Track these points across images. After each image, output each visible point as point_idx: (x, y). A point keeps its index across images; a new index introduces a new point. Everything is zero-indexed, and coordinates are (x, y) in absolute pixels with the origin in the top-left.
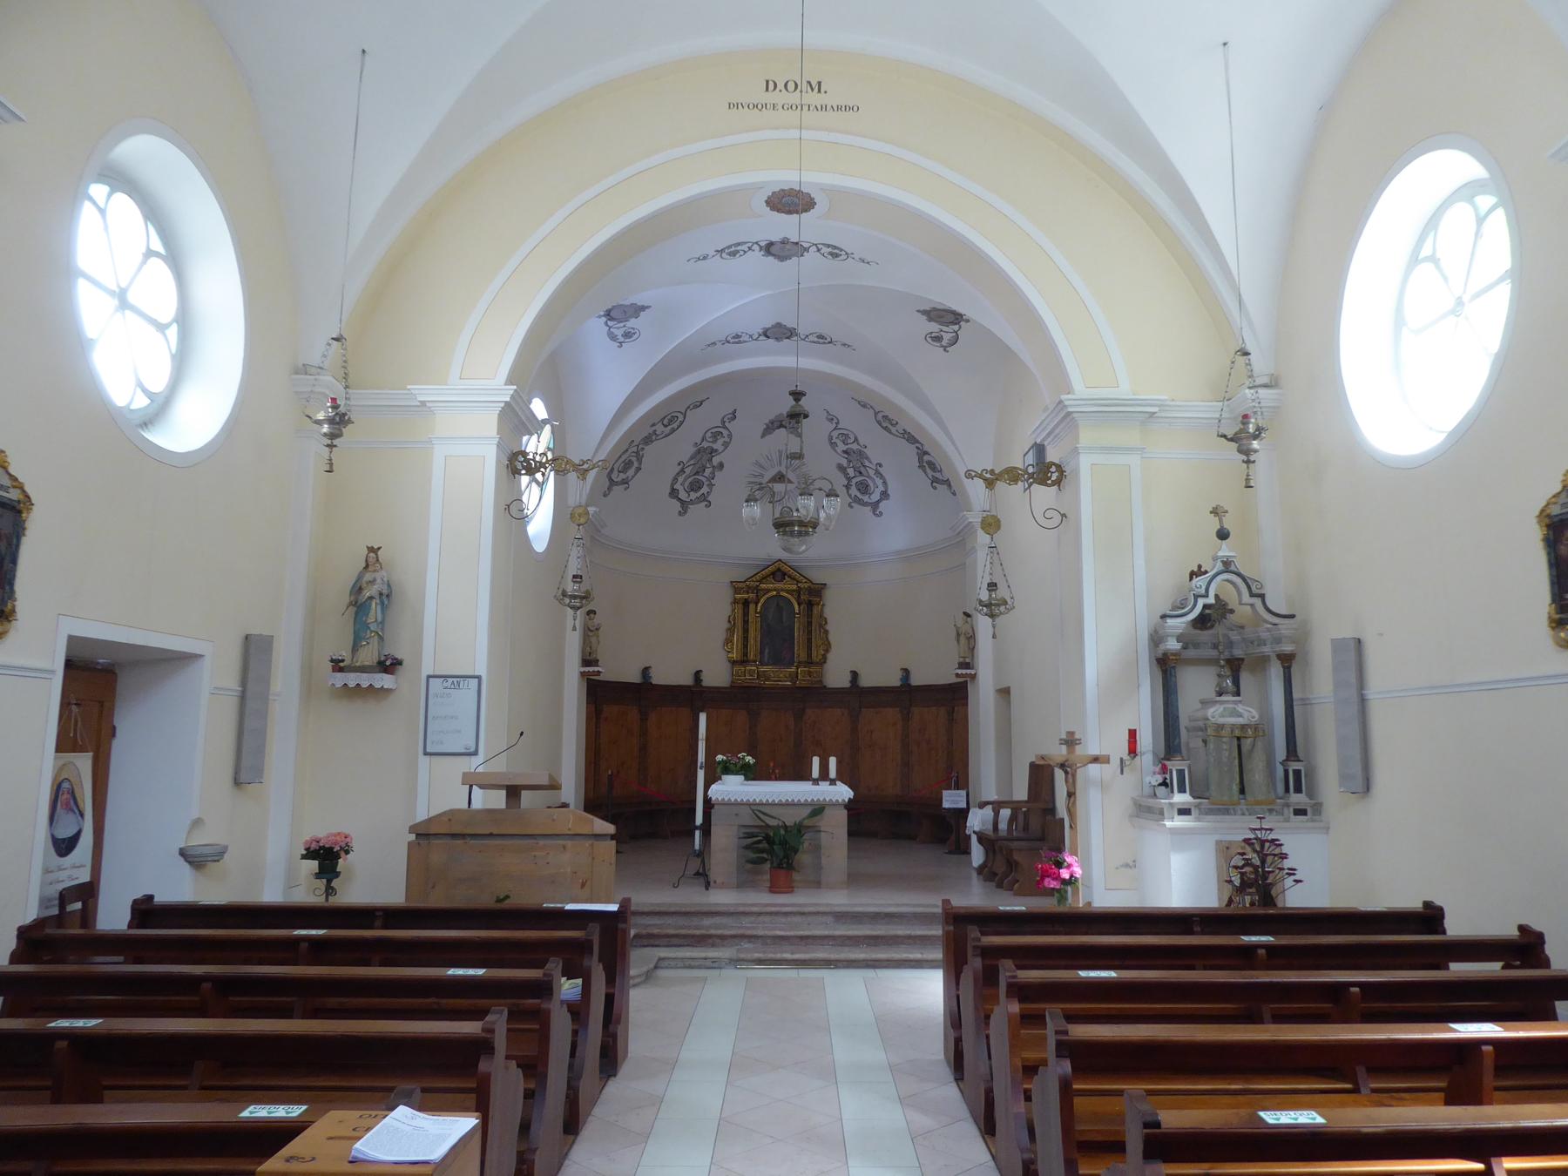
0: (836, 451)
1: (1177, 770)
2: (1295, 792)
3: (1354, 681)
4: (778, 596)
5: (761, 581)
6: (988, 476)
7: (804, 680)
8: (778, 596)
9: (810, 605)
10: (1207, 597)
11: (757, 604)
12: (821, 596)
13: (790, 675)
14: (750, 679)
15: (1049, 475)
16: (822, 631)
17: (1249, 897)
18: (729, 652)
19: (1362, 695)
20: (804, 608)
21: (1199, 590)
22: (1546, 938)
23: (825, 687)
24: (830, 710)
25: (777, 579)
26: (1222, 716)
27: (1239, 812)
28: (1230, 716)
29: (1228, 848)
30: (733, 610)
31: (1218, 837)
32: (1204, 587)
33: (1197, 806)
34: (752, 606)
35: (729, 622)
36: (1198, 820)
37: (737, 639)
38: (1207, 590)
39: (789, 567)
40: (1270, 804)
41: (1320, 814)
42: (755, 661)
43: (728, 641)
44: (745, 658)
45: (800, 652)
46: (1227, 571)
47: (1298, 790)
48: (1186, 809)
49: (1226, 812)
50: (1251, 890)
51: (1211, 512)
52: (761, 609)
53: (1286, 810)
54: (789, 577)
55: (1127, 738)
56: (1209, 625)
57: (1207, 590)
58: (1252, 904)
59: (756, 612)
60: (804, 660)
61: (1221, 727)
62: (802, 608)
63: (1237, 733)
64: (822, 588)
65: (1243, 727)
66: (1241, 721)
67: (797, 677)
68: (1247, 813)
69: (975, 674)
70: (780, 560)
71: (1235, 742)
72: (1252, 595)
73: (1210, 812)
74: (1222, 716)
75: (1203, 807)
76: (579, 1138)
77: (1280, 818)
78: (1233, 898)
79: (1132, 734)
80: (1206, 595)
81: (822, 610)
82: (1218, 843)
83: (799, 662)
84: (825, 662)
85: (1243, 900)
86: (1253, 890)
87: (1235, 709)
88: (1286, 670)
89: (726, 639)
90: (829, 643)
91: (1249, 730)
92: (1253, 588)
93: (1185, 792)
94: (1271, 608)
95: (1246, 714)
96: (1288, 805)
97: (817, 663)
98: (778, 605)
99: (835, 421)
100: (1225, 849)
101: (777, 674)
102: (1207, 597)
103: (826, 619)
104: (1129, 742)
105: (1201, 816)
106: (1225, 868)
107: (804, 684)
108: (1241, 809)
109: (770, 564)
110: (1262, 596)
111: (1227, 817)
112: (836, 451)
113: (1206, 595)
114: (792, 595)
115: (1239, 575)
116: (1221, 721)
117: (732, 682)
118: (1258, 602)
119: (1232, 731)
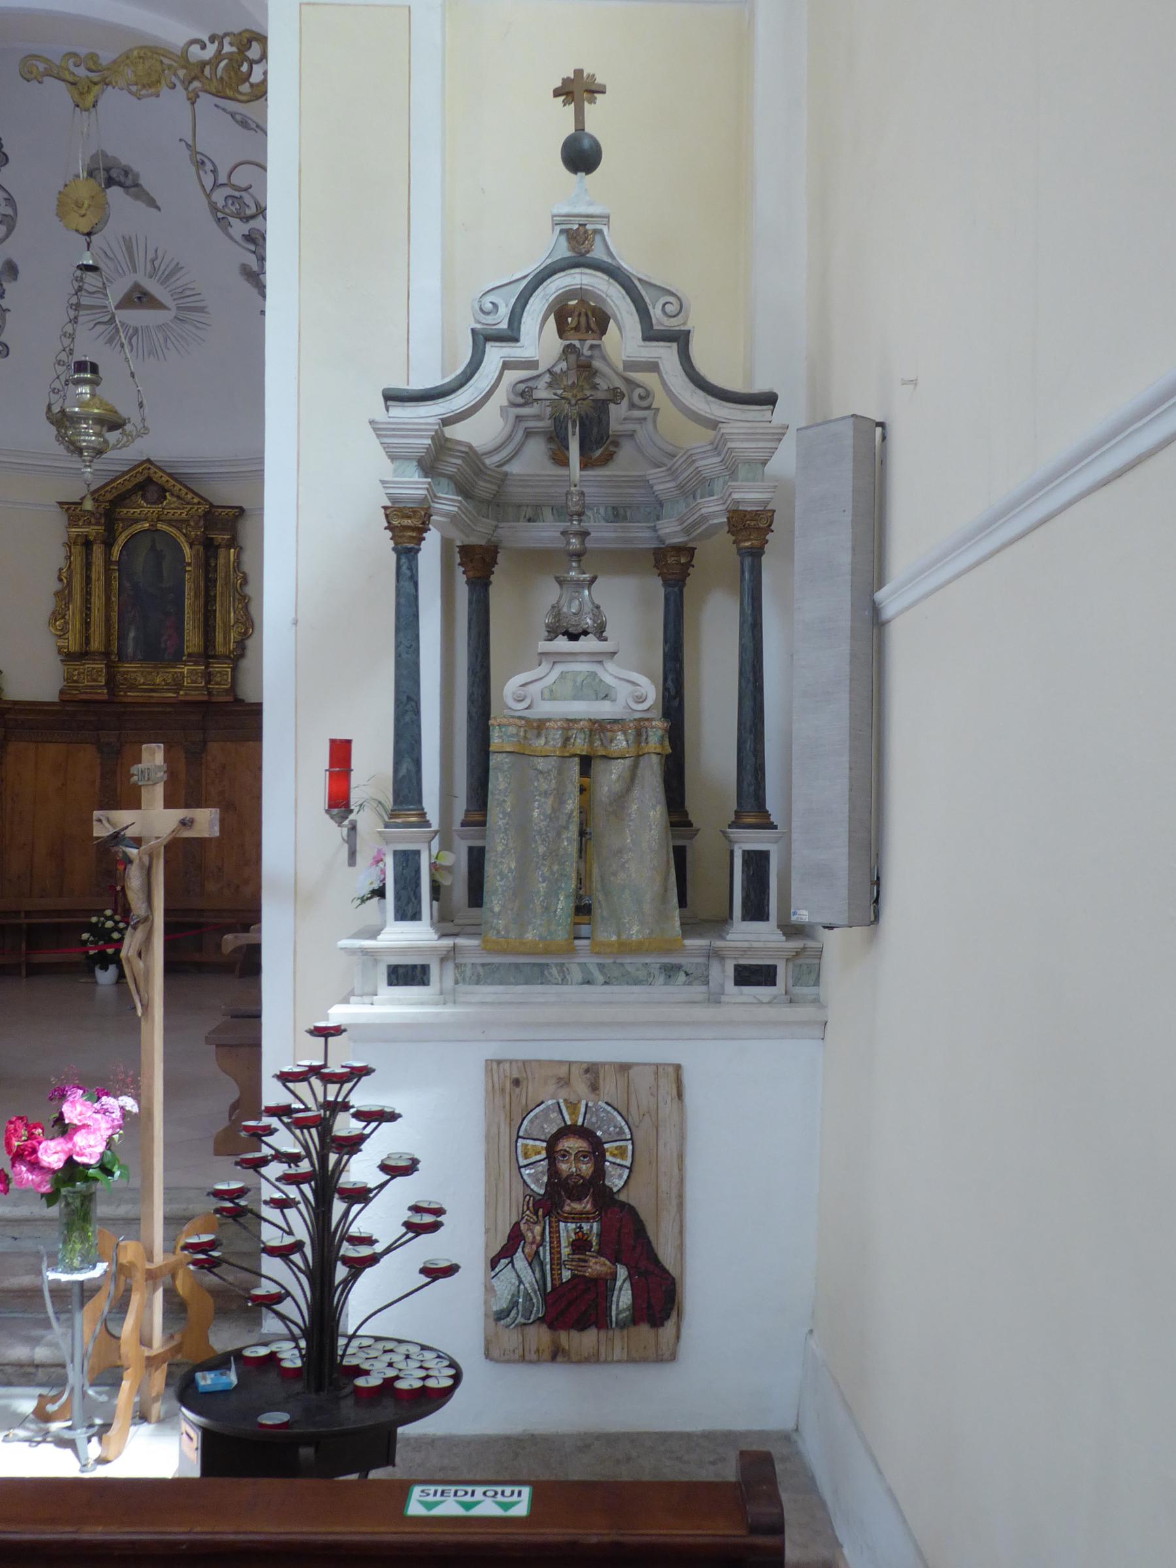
0: (231, 237)
1: (395, 853)
2: (744, 919)
3: (845, 559)
4: (153, 531)
5: (580, 603)
6: (82, 72)
8: (153, 531)
9: (210, 548)
10: (517, 340)
11: (109, 545)
14: (92, 687)
15: (245, 68)
17: (572, 1226)
19: (876, 609)
21: (490, 319)
25: (148, 495)
26: (551, 695)
27: (576, 974)
28: (575, 698)
29: (517, 1082)
30: (68, 558)
31: (494, 1050)
32: (504, 311)
33: (450, 955)
34: (98, 551)
35: (60, 580)
36: (446, 997)
38: (516, 317)
40: (668, 952)
41: (817, 983)
43: (58, 615)
45: (192, 640)
46: (579, 261)
47: (756, 910)
48: (414, 967)
49: (537, 974)
50: (577, 1206)
51: (557, 93)
53: (715, 970)
54: (172, 495)
55: (326, 764)
56: (598, 453)
57: (516, 317)
58: (580, 1245)
61: (539, 726)
63: (580, 745)
65: (598, 728)
66: (604, 710)
68: (600, 978)
70: (148, 461)
71: (575, 767)
72: (651, 335)
73: (487, 975)
74: (551, 695)
75: (468, 961)
76: (481, 1312)
77: (698, 990)
78: (523, 1227)
79: (341, 752)
80: (511, 336)
82: (494, 1064)
84: (242, 656)
85: (555, 1233)
86: (586, 1205)
87: (593, 675)
88: (748, 561)
89: (53, 613)
91: (620, 736)
92: (656, 313)
93: (416, 916)
94: (237, 169)
95: (623, 692)
96: (715, 955)
98: (153, 548)
99: (209, 167)
100: (508, 1084)
102: (517, 340)
104: (332, 776)
105: (462, 987)
106: (505, 1140)
107: (195, 696)
108: (583, 966)
109: (126, 469)
110: (681, 339)
111: (536, 991)
112: (231, 237)
113: (511, 336)
115: (614, 272)
116: (546, 709)
118: (667, 354)
119: (567, 740)
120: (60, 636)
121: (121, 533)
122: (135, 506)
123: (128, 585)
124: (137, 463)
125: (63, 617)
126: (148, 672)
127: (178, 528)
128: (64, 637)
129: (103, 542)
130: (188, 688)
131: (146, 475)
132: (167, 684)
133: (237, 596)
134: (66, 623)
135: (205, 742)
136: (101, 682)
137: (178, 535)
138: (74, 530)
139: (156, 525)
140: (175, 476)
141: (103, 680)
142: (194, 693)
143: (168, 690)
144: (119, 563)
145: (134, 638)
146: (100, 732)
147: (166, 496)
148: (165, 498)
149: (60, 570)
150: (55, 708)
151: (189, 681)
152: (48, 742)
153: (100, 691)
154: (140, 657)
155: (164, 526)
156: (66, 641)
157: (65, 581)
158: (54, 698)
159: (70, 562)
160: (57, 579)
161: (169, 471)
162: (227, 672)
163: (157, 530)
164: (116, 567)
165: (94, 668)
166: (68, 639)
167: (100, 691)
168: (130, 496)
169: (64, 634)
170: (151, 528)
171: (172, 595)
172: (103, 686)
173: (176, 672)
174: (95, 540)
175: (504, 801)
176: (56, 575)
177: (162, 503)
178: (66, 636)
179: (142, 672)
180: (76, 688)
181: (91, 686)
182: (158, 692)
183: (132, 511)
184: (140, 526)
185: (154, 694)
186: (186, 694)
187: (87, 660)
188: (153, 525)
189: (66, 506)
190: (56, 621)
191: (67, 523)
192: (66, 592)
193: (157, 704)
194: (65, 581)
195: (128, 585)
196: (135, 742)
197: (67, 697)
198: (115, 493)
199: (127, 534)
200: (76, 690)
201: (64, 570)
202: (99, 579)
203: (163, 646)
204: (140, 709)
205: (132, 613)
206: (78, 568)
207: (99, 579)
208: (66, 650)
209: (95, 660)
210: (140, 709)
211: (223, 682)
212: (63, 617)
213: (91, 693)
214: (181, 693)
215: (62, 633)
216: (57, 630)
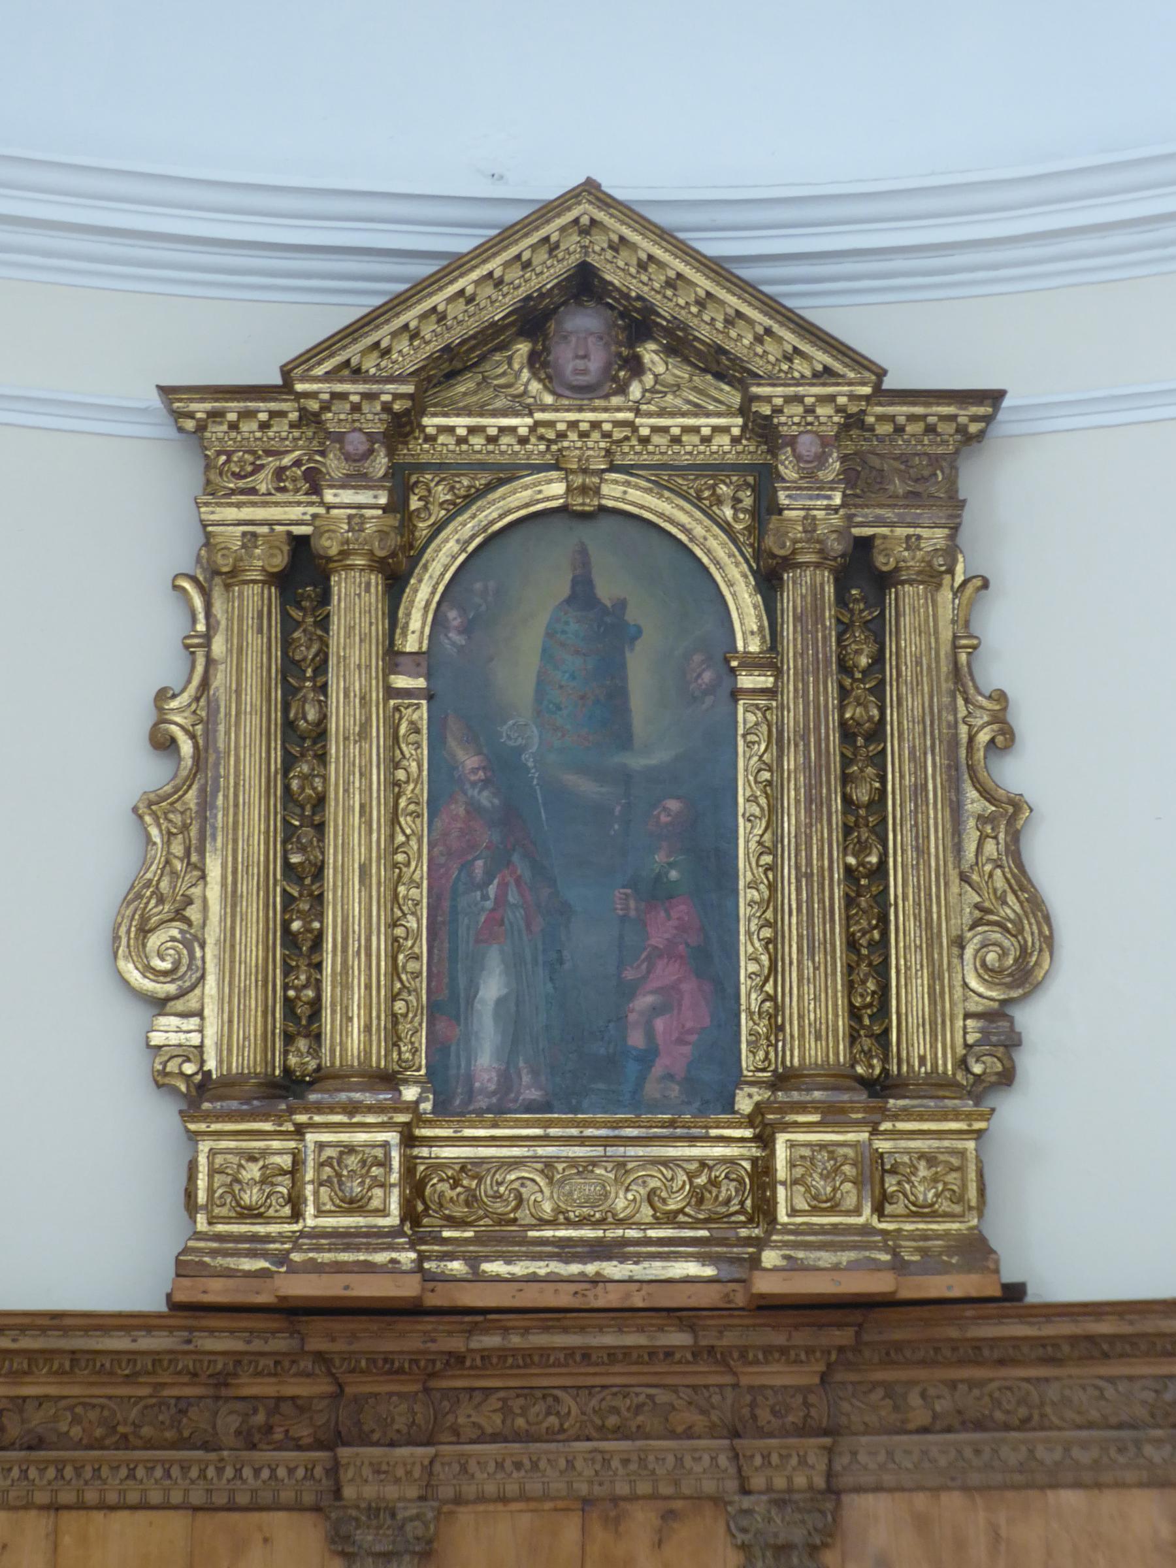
7: (834, 1238)
12: (954, 504)
13: (698, 1197)
16: (974, 802)
18: (161, 1005)
20: (816, 593)
22: (594, 177)
23: (1014, 1292)
24: (1070, 1498)
25: (565, 356)
35: (164, 744)
37: (232, 898)
39: (716, 268)
42: (390, 1080)
44: (300, 1059)
52: (438, 623)
59: (393, 658)
60: (814, 1052)
62: (792, 598)
64: (969, 440)
67: (764, 1211)
69: (190, 1239)
81: (964, 624)
83: (783, 1079)
84: (1007, 1078)
89: (133, 896)
90: (1035, 905)
97: (938, 1085)
101: (584, 1188)
103: (1001, 697)
109: (463, 245)
114: (705, 505)
117: (184, 1268)
120: (168, 999)
121: (438, 528)
122: (499, 403)
123: (469, 761)
124: (515, 215)
125: (179, 915)
126: (572, 1162)
127: (696, 501)
128: (179, 1005)
129: (380, 565)
130: (804, 1237)
131: (573, 260)
132: (671, 1219)
133: (974, 802)
134: (193, 940)
135: (833, 1491)
136: (383, 1212)
137: (699, 531)
138: (231, 513)
139: (597, 491)
140: (746, 273)
141: (394, 1207)
142: (826, 1258)
143: (669, 1249)
144: (425, 662)
145: (500, 1002)
146: (344, 1452)
147: (638, 359)
148: (636, 367)
149: (163, 696)
150: (146, 1343)
151: (802, 1205)
152: (103, 1506)
153: (381, 1258)
154: (533, 1094)
155: (634, 495)
156: (194, 1022)
157: (186, 747)
158: (151, 1301)
159: (210, 662)
160: (149, 746)
161: (711, 248)
162: (962, 1153)
163: (603, 509)
164: (421, 683)
165: (350, 1149)
166: (200, 1014)
167: (381, 1258)
168: (483, 358)
169: (182, 994)
170: (577, 503)
171: (673, 805)
172: (397, 1232)
173: (703, 1163)
174: (344, 554)
175: (594, 1411)
176: (143, 719)
177: (622, 390)
178: (192, 1002)
179: (548, 1165)
180: (255, 1245)
181: (335, 1234)
182: (623, 1258)
183: (492, 424)
184: (526, 495)
185: (613, 1270)
186: (793, 1266)
187: (319, 1108)
188: (584, 490)
189: (200, 408)
190: (144, 931)
191: (198, 490)
192: (191, 797)
193: (623, 1314)
194: (186, 747)
195: (469, 761)
196: (503, 1499)
197: (216, 1291)
198: (434, 340)
199: (467, 531)
200: (252, 1254)
201: (185, 699)
202: (364, 733)
203: (636, 1039)
204: (540, 1340)
205: (492, 890)
206: (252, 695)
207: (364, 733)
208: (189, 1068)
209: (352, 1109)
210: (540, 1340)
211: (944, 1206)
212: (179, 915)
213: (339, 1268)
214: (770, 1258)
215: (172, 988)
216: (148, 970)
